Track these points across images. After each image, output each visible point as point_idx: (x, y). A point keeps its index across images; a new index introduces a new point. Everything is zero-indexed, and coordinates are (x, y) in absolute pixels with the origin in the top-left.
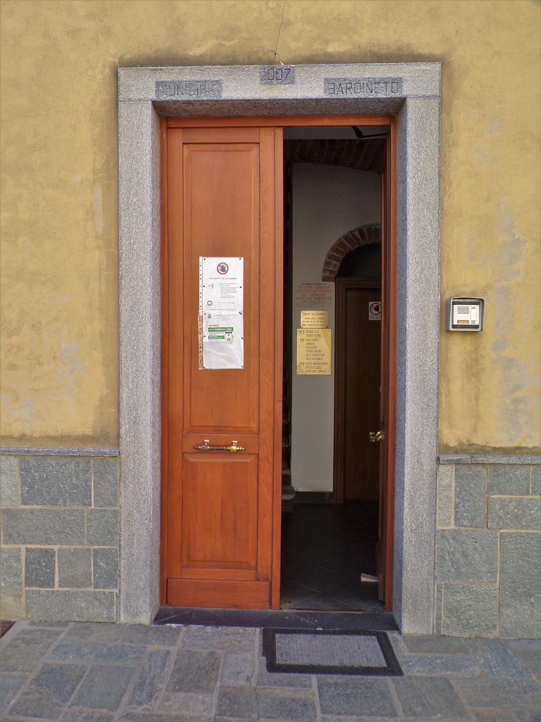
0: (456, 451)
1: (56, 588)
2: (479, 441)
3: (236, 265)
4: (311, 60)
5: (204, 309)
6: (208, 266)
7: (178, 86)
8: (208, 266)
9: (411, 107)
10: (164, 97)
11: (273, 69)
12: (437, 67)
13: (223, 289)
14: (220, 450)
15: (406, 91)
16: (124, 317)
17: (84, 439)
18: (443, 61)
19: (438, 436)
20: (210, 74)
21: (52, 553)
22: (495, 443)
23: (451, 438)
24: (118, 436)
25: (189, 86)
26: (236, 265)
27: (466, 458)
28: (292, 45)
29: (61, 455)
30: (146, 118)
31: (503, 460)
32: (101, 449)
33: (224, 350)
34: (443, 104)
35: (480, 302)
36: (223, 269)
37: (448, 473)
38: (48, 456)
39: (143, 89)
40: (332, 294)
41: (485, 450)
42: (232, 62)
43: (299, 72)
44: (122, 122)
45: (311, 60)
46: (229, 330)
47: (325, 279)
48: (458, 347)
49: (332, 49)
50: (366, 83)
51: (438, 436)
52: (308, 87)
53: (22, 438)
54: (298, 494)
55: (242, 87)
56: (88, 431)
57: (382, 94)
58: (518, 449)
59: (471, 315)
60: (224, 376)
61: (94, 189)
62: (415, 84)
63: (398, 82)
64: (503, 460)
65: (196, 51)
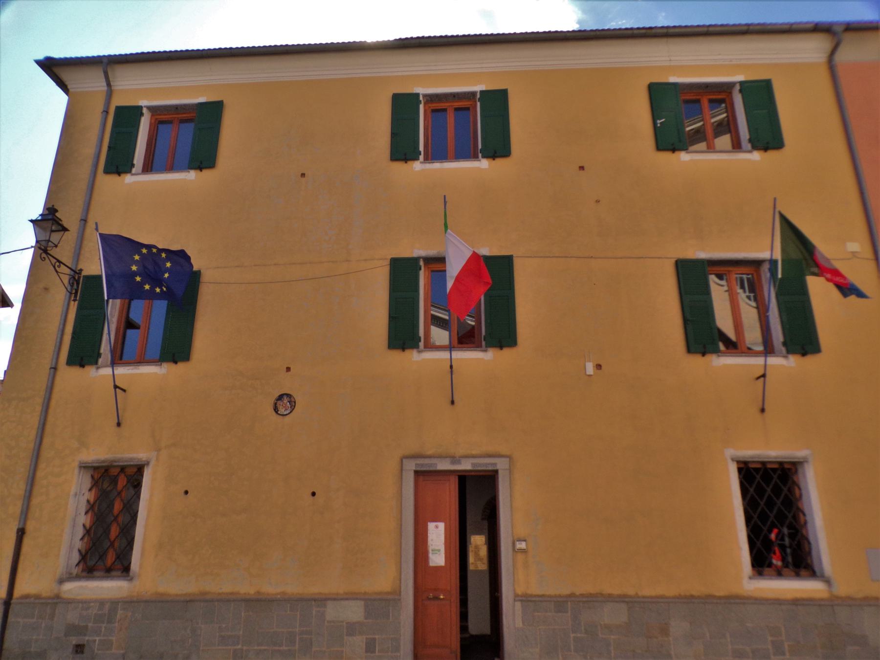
0: (522, 596)
1: (377, 654)
2: (529, 592)
3: (442, 526)
4: (467, 457)
5: (430, 542)
6: (431, 526)
7: (422, 465)
8: (431, 526)
9: (500, 472)
10: (418, 469)
11: (454, 459)
12: (508, 459)
13: (437, 535)
14: (436, 598)
15: (498, 467)
16: (403, 546)
17: (388, 593)
18: (509, 457)
19: (514, 590)
20: (433, 461)
21: (374, 639)
22: (534, 593)
23: (519, 592)
24: (400, 592)
25: (426, 464)
26: (442, 526)
27: (526, 599)
28: (461, 451)
29: (380, 600)
30: (412, 475)
31: (537, 599)
32: (390, 600)
33: (438, 558)
34: (510, 471)
35: (525, 541)
36: (437, 527)
37: (518, 605)
38: (375, 600)
39: (411, 466)
40: (486, 527)
41: (531, 596)
42: (440, 457)
43: (463, 461)
44: (404, 477)
45: (467, 457)
46: (439, 550)
47: (483, 519)
48: (520, 557)
49: (474, 452)
50: (484, 464)
51: (514, 590)
52: (466, 466)
53: (365, 593)
54: (472, 636)
55: (444, 465)
56: (389, 589)
57: (490, 468)
58: (543, 596)
59: (523, 545)
60: (438, 568)
61: (392, 499)
62: (501, 465)
63: (495, 464)
64: (537, 599)
65: (430, 452)
